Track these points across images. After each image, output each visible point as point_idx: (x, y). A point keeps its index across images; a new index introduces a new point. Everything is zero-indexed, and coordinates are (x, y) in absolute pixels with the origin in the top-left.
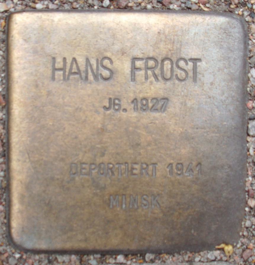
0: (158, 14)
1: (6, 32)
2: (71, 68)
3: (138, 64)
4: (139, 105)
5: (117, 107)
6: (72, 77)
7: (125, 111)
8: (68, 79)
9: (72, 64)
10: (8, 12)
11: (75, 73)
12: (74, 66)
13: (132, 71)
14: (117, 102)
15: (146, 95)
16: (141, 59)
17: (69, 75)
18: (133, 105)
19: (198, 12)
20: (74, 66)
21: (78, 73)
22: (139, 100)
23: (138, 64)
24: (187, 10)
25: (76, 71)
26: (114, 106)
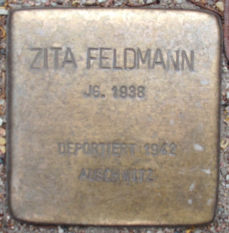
0: (207, 14)
1: (7, 22)
2: (155, 58)
3: (94, 53)
4: (119, 93)
5: (96, 94)
6: (67, 65)
7: (103, 97)
8: (153, 67)
9: (156, 55)
10: (19, 3)
11: (69, 62)
12: (69, 56)
13: (88, 59)
14: (96, 89)
15: (123, 83)
16: (96, 49)
17: (153, 65)
18: (113, 92)
19: (144, 8)
20: (69, 56)
21: (162, 62)
22: (118, 88)
23: (94, 53)
24: (129, 6)
25: (71, 60)
26: (94, 93)
